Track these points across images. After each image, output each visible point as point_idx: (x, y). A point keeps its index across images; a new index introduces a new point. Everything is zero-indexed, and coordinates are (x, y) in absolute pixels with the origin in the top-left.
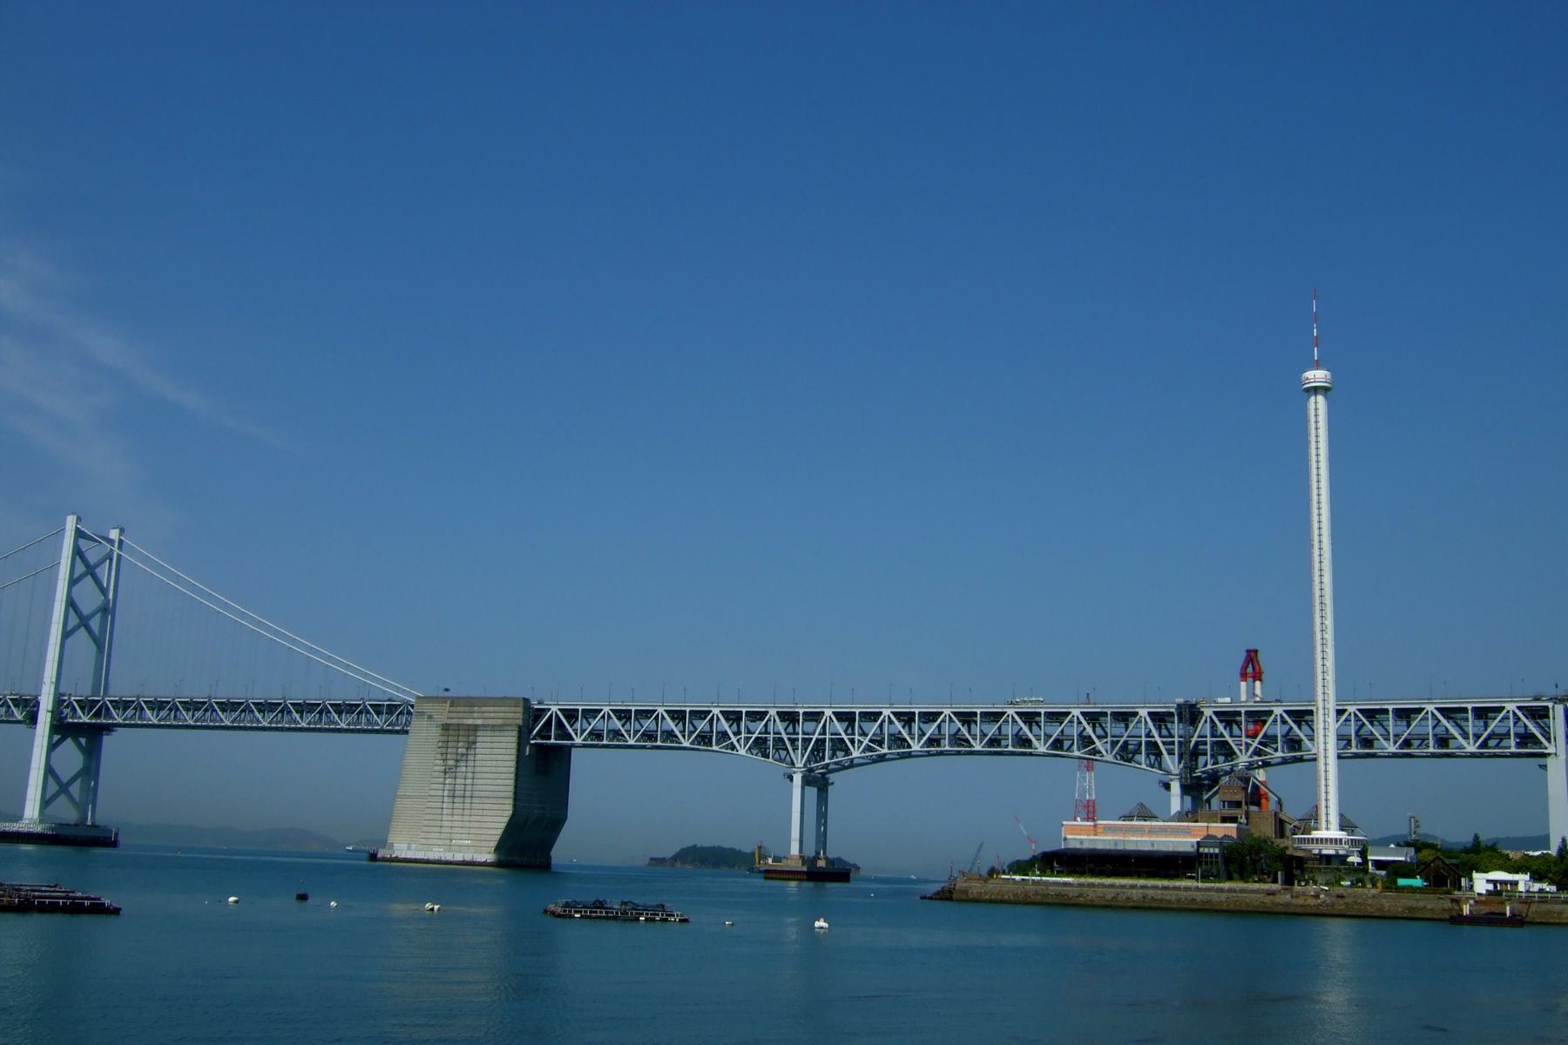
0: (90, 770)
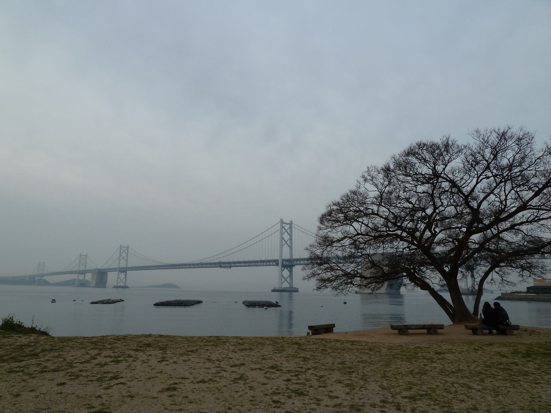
0: (291, 276)
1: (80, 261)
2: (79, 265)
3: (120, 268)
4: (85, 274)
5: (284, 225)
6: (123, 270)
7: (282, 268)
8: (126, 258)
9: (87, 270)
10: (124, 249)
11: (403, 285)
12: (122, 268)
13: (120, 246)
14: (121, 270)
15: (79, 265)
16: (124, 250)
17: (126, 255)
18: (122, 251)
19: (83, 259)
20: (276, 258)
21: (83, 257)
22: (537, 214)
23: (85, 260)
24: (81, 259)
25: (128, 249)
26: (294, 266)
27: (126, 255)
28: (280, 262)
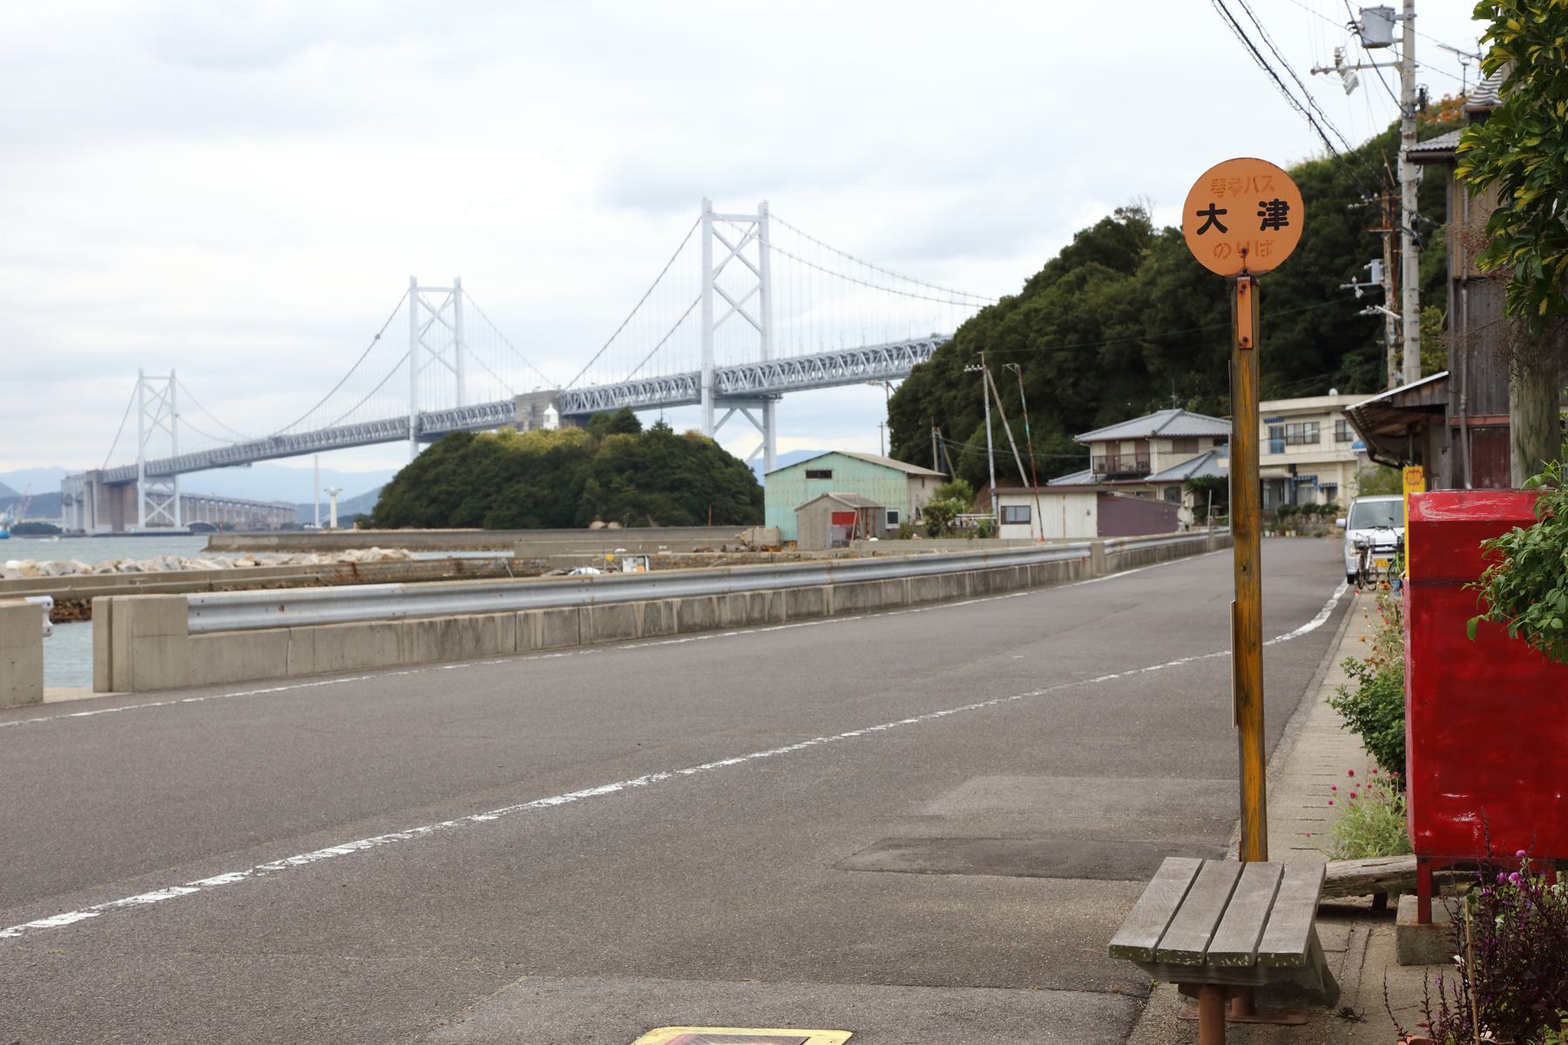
1: (710, 273)
2: (707, 312)
3: (147, 465)
4: (764, 399)
5: (718, 225)
6: (745, 386)
7: (711, 414)
8: (753, 307)
9: (788, 367)
10: (733, 234)
11: (1295, 474)
12: (732, 374)
13: (408, 285)
14: (728, 387)
15: (707, 312)
16: (437, 305)
17: (757, 280)
18: (719, 252)
19: (436, 315)
20: (687, 367)
21: (437, 300)
22: (436, 356)
23: (451, 321)
24: (450, 310)
25: (457, 302)
26: (776, 394)
27: (720, 281)
28: (706, 381)
